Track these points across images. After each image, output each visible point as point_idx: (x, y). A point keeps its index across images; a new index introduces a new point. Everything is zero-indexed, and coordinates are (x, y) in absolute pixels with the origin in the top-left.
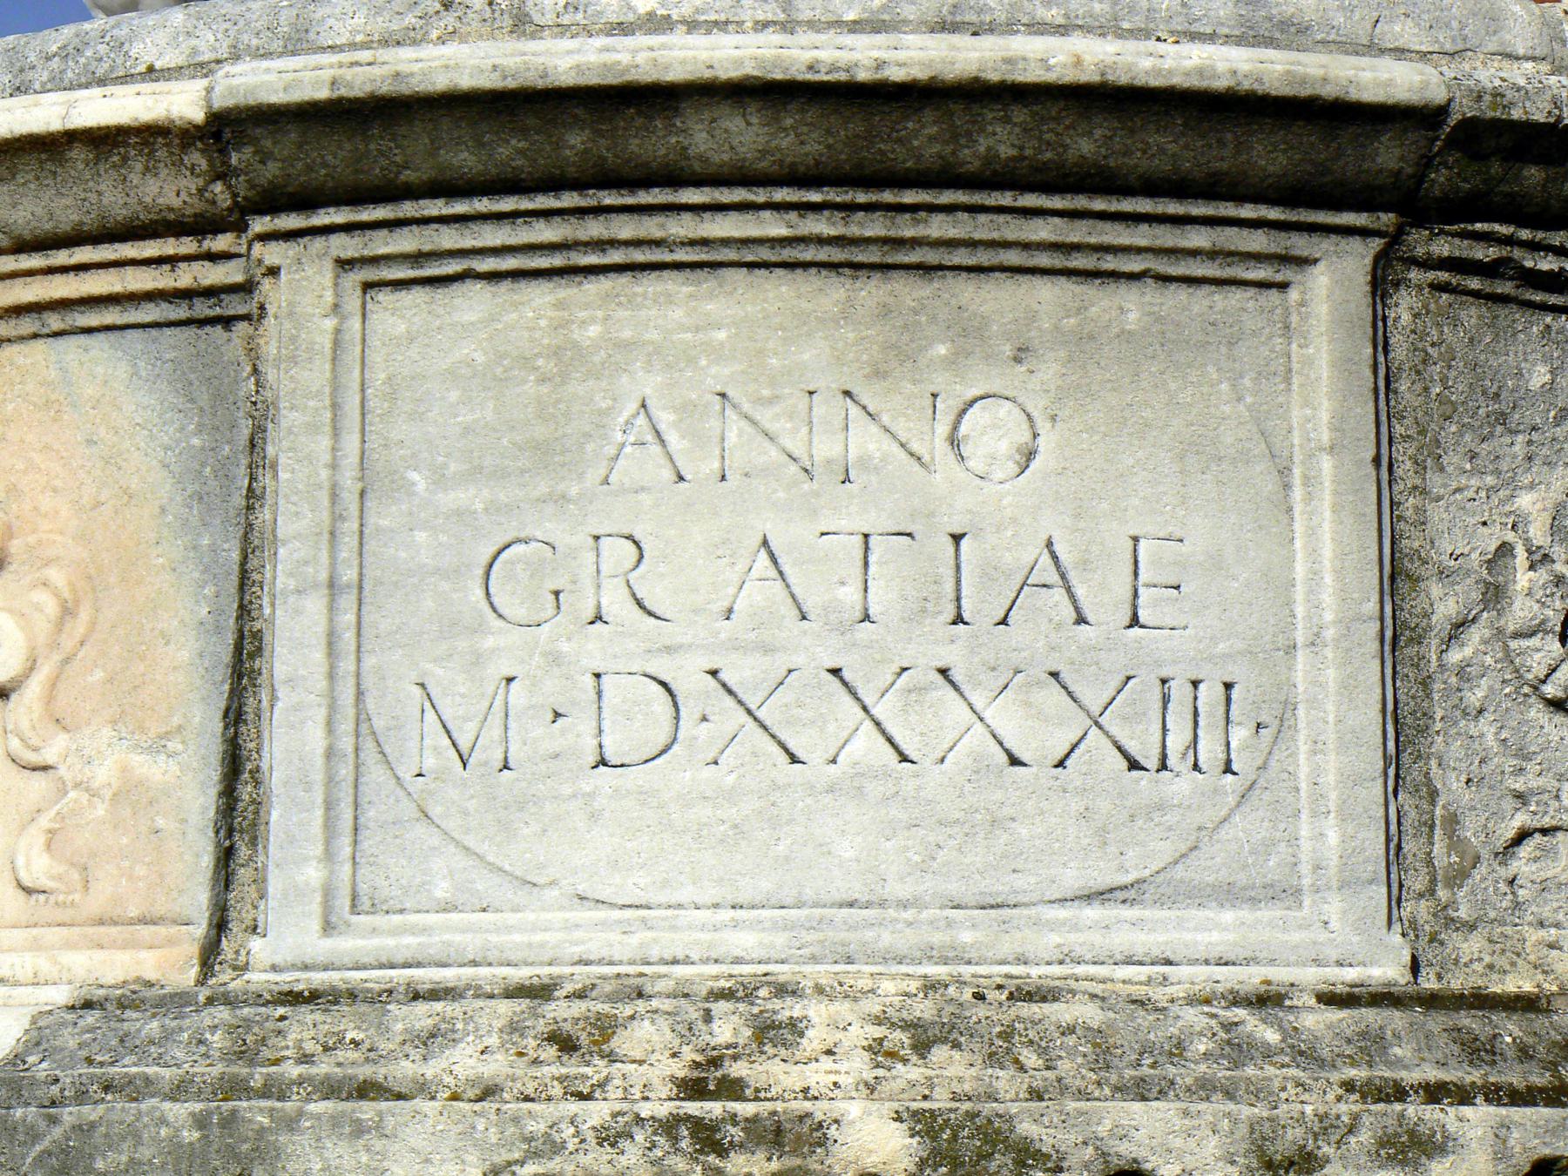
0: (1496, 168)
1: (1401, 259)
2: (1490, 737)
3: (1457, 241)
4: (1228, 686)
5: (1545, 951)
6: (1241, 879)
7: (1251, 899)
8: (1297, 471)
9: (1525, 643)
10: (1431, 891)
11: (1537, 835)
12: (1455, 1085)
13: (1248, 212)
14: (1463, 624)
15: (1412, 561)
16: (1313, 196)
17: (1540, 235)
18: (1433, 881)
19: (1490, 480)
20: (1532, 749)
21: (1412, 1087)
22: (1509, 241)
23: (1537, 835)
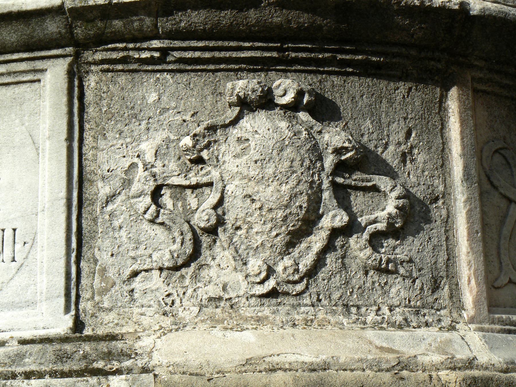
0: (100, 24)
1: (84, 63)
2: (125, 237)
3: (104, 53)
4: (14, 230)
5: (139, 317)
6: (17, 300)
7: (20, 307)
8: (40, 148)
9: (137, 200)
10: (93, 298)
11: (143, 273)
12: (37, 371)
13: (15, 56)
14: (114, 196)
15: (90, 175)
16: (36, 46)
17: (138, 45)
18: (93, 294)
19: (128, 140)
20: (142, 240)
21: (19, 373)
22: (125, 49)
23: (143, 273)
